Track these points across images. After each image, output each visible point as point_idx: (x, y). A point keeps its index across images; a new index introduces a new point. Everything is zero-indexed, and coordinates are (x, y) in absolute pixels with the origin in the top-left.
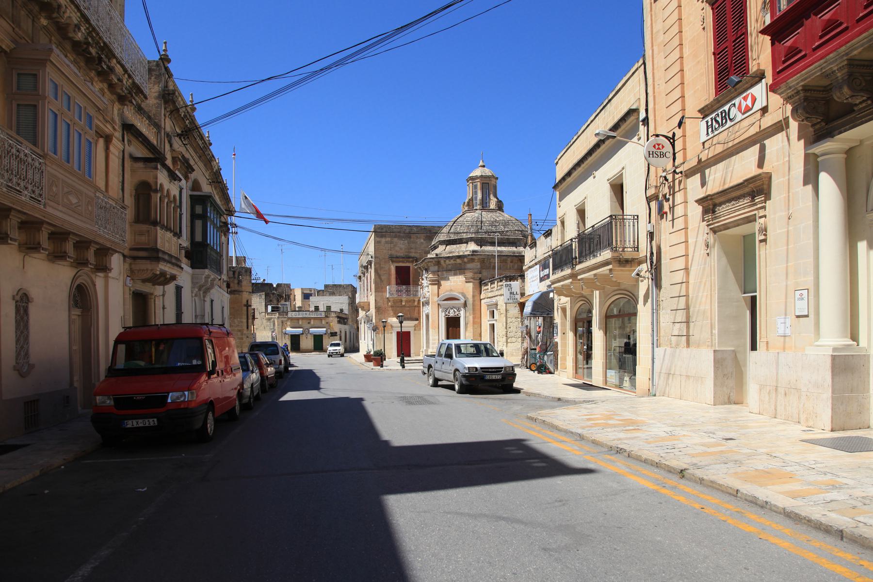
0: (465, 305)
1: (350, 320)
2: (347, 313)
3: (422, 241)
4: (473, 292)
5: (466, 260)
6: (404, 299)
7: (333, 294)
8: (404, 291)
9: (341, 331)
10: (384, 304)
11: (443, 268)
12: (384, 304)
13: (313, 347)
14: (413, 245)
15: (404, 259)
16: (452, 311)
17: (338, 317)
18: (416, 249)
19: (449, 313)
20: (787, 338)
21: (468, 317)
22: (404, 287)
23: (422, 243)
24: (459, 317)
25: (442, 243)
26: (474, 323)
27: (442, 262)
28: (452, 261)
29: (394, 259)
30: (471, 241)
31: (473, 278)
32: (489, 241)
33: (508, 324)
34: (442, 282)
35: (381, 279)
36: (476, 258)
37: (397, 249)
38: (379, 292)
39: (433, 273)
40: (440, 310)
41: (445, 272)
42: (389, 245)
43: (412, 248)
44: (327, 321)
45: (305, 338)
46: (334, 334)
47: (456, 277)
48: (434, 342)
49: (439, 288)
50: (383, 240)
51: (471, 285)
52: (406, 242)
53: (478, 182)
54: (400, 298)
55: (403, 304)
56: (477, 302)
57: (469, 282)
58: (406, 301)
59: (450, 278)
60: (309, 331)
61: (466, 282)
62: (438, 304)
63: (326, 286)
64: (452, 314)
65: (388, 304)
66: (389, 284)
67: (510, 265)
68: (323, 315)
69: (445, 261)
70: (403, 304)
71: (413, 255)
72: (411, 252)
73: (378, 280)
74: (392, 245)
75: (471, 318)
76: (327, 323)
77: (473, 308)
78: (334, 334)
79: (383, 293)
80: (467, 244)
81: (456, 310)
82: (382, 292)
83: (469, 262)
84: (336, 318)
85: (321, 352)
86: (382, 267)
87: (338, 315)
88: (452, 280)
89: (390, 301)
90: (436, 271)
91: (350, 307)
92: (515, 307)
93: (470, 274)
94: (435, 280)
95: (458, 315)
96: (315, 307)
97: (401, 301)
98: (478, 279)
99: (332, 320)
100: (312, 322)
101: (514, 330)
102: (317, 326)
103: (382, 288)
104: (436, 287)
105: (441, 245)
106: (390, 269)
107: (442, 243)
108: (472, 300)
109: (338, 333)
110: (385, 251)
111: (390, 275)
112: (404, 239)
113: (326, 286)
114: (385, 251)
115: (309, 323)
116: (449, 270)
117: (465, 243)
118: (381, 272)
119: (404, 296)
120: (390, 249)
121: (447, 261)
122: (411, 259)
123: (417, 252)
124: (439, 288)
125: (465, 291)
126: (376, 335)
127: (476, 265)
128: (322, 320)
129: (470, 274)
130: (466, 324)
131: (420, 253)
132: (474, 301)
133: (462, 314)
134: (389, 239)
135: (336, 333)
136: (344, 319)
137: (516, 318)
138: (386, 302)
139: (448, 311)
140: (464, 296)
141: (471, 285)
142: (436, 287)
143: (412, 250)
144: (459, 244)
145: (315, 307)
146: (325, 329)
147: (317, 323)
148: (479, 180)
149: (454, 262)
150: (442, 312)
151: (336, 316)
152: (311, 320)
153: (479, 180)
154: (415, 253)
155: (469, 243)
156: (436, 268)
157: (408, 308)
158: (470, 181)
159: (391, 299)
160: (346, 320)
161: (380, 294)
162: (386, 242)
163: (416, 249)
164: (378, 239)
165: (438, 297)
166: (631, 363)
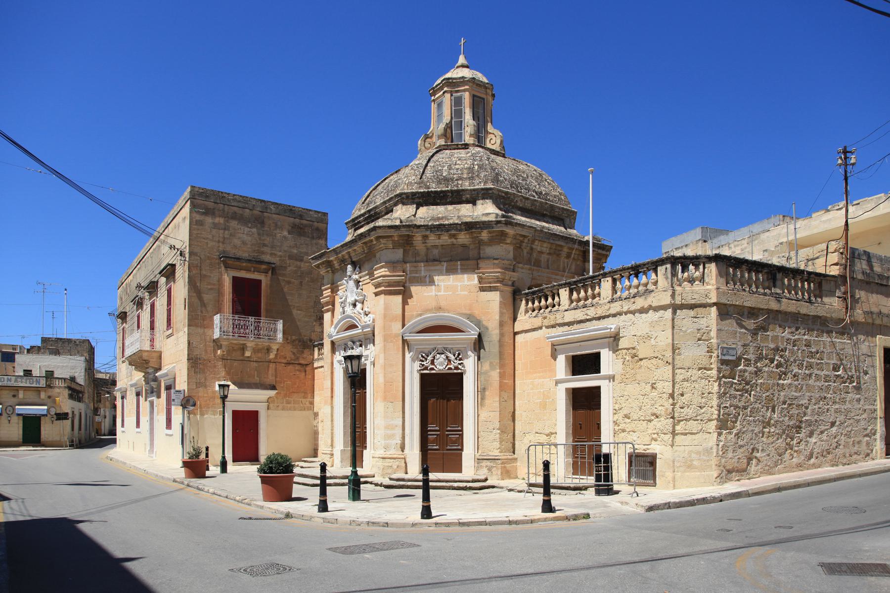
0: (479, 344)
1: (86, 395)
2: (82, 383)
3: (285, 233)
4: (501, 314)
5: (485, 235)
6: (249, 344)
7: (56, 352)
8: (252, 328)
9: (73, 412)
10: (206, 351)
11: (416, 254)
12: (206, 351)
13: (21, 437)
14: (268, 240)
15: (249, 265)
16: (441, 358)
17: (70, 388)
18: (273, 247)
19: (433, 362)
20: (670, 436)
21: (486, 373)
22: (252, 319)
23: (285, 237)
24: (461, 375)
25: (405, 199)
26: (502, 387)
27: (418, 238)
28: (445, 239)
29: (230, 262)
30: (483, 198)
31: (501, 281)
32: (520, 204)
33: (677, 386)
34: (414, 289)
35: (200, 298)
36: (510, 231)
37: (237, 242)
38: (197, 326)
39: (392, 265)
40: (408, 356)
41: (422, 264)
42: (221, 231)
43: (265, 245)
44: (50, 394)
45: (7, 421)
46: (62, 416)
47: (452, 277)
48: (390, 432)
49: (405, 303)
50: (209, 220)
51: (494, 298)
52: (254, 230)
53: (464, 91)
54: (242, 341)
55: (248, 354)
56: (508, 339)
57: (491, 289)
58: (256, 350)
59: (436, 278)
60: (14, 409)
61: (482, 289)
62: (404, 341)
63: (45, 340)
64: (440, 365)
65: (215, 352)
66: (219, 311)
67: (564, 263)
68: (43, 383)
69: (425, 237)
70: (248, 354)
71: (267, 258)
72: (263, 253)
73: (196, 300)
74: (227, 232)
75: (495, 375)
76: (49, 397)
77: (500, 352)
78: (62, 416)
79: (206, 330)
80: (474, 204)
81: (452, 357)
82: (204, 327)
83: (492, 242)
84: (67, 390)
85: (37, 446)
86: (205, 276)
87: (69, 385)
88: (442, 284)
89: (220, 347)
90: (398, 262)
91: (87, 377)
92: (699, 340)
93: (493, 271)
94: (397, 283)
95: (457, 368)
96: (24, 371)
97: (243, 348)
98: (510, 283)
99: (59, 393)
100: (21, 394)
101: (697, 400)
102: (30, 401)
103: (204, 320)
104: (399, 299)
105: (404, 204)
106: (220, 282)
107: (405, 199)
108: (497, 331)
109: (70, 415)
110: (211, 244)
111: (220, 293)
112: (250, 225)
113: (45, 340)
114: (211, 244)
115: (14, 396)
116: (435, 260)
117: (468, 202)
118: (203, 286)
119: (251, 337)
120: (221, 240)
121: (433, 239)
122: (264, 267)
123: (275, 255)
124: (405, 303)
125: (477, 313)
126: (189, 417)
127: (504, 250)
128: (39, 391)
129: (493, 271)
130: (481, 392)
131: (281, 256)
132: (502, 335)
133: (469, 364)
134: (222, 220)
135: (67, 414)
136: (78, 392)
137: (700, 369)
138: (210, 349)
139: (430, 358)
140: (478, 323)
141: (494, 298)
142: (399, 299)
143: (265, 249)
144: (451, 203)
145: (24, 371)
146: (46, 407)
147: (31, 396)
148: (467, 87)
149: (449, 241)
150: (413, 360)
151: (66, 385)
152: (18, 390)
153: (467, 87)
154: (271, 254)
155: (479, 202)
156: (399, 254)
157: (255, 364)
158: (446, 89)
159: (224, 343)
160: (81, 395)
161: (200, 330)
162: (215, 226)
163: (273, 247)
164: (198, 217)
165: (403, 326)
166: (651, 474)
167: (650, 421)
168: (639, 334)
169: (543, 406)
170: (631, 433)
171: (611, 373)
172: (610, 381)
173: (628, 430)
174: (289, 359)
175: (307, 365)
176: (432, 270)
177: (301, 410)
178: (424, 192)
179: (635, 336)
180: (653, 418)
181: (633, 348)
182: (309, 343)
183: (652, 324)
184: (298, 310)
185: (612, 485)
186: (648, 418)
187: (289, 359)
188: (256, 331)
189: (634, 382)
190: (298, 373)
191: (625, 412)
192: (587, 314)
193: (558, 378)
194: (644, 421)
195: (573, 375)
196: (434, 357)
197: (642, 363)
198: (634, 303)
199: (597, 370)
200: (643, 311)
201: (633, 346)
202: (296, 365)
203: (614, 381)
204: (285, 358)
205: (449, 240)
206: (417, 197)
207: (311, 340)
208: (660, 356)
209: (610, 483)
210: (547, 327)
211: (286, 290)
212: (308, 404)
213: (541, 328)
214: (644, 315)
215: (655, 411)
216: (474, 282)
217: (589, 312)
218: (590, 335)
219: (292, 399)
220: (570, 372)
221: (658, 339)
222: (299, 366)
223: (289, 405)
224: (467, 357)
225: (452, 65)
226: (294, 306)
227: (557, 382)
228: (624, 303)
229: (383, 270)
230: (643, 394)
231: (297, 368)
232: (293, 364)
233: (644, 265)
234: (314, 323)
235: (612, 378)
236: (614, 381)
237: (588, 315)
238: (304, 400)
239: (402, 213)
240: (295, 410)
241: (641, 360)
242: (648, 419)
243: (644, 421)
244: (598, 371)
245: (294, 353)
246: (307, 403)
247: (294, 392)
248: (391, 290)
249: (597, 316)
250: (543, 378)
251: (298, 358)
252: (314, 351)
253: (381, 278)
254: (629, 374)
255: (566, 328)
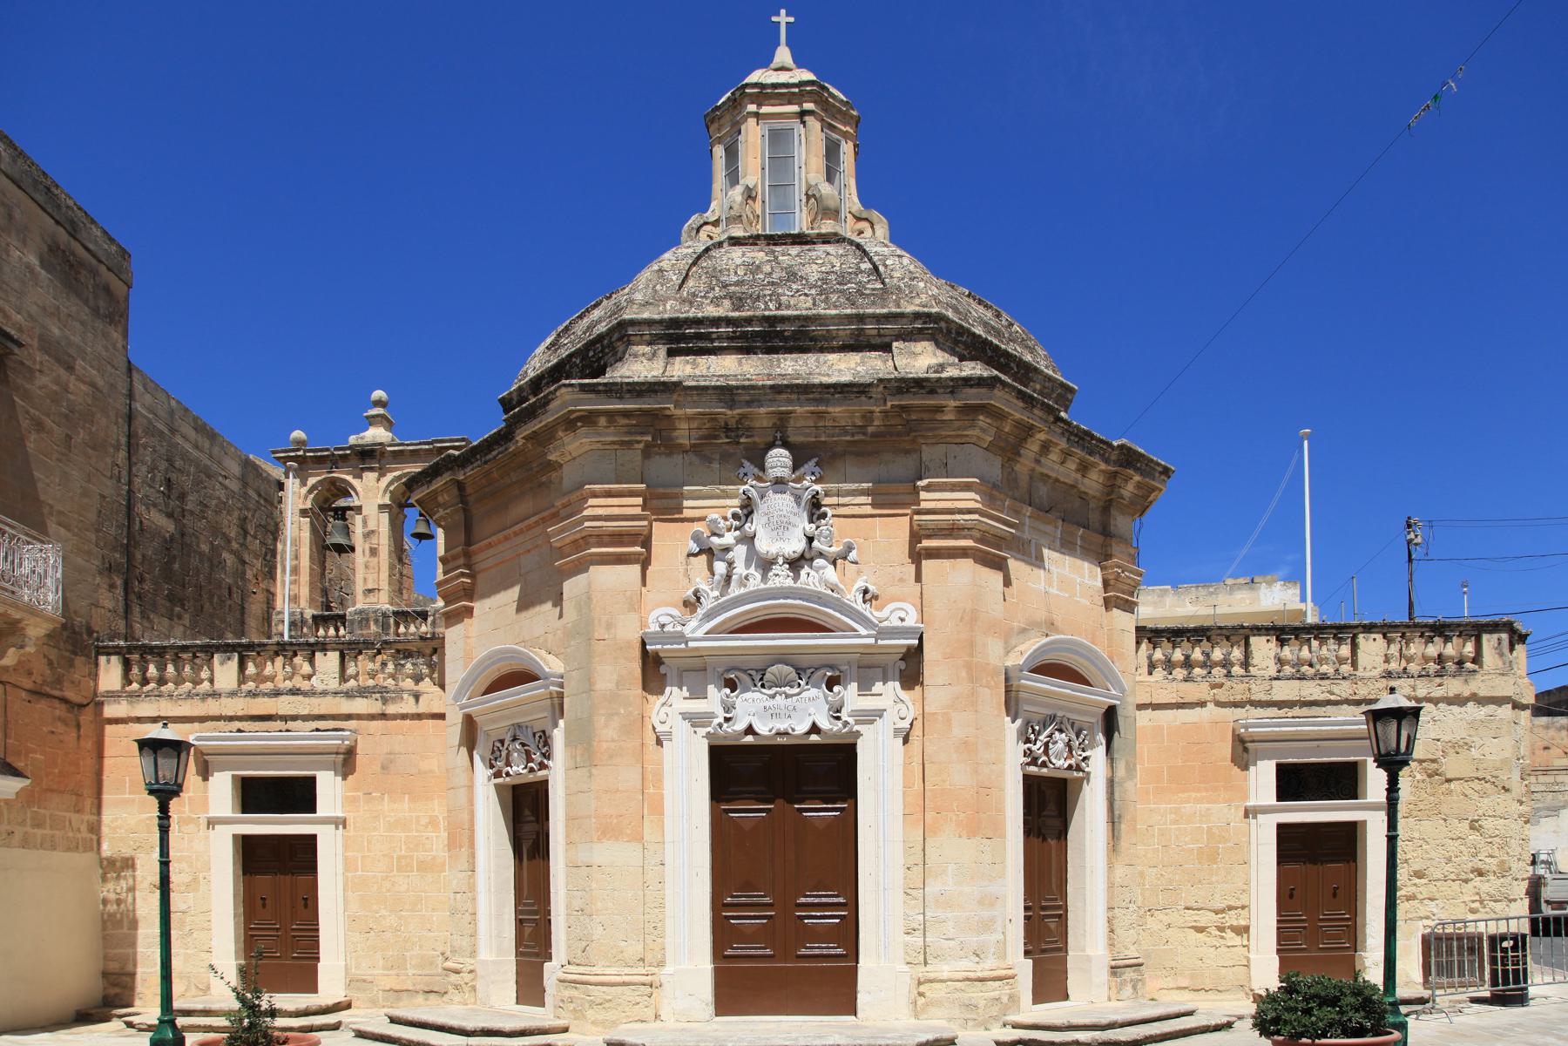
3: (33, 260)
167: (1466, 881)
168: (1446, 738)
169: (1210, 856)
170: (1426, 902)
171: (340, 814)
172: (337, 828)
173: (1419, 896)
174: (39, 680)
175: (82, 706)
176: (1040, 531)
177: (68, 849)
178: (980, 336)
179: (1438, 740)
180: (1472, 876)
181: (1434, 761)
182: (85, 636)
183: (1473, 725)
184: (60, 524)
185: (1526, 989)
186: (1464, 876)
187: (39, 680)
188: (40, 570)
189: (1435, 817)
190: (60, 728)
191: (1416, 867)
192: (1332, 693)
193: (211, 815)
194: (1453, 881)
195: (244, 812)
196: (1050, 736)
197: (1453, 785)
198: (1439, 686)
199: (310, 806)
200: (1459, 701)
201: (1434, 757)
202: (57, 703)
203: (345, 827)
204: (30, 673)
205: (1074, 475)
206: (965, 343)
207: (90, 632)
208: (1489, 777)
209: (1522, 985)
210: (1219, 704)
211: (31, 446)
212: (85, 834)
213: (1202, 704)
214: (1455, 709)
215: (1480, 865)
216: (1095, 583)
217: (1336, 689)
218: (1297, 731)
219: (47, 813)
220: (239, 808)
221: (1486, 750)
222: (63, 706)
223: (39, 832)
224: (1092, 746)
225: (765, 61)
226: (51, 507)
227: (211, 823)
228: (1420, 683)
229: (971, 495)
230: (1454, 837)
231: (57, 712)
232: (49, 696)
233: (1459, 625)
234: (98, 580)
235: (341, 823)
236: (345, 827)
237: (1333, 694)
238: (75, 817)
239: (642, 366)
240: (54, 848)
241: (1449, 781)
242: (1464, 877)
243: (1453, 881)
244: (313, 809)
245: (50, 663)
246: (84, 828)
247: (52, 791)
248: (988, 553)
249: (1357, 697)
250: (1209, 803)
251: (59, 681)
252: (97, 665)
253: (976, 517)
254: (1425, 802)
255: (1273, 711)
